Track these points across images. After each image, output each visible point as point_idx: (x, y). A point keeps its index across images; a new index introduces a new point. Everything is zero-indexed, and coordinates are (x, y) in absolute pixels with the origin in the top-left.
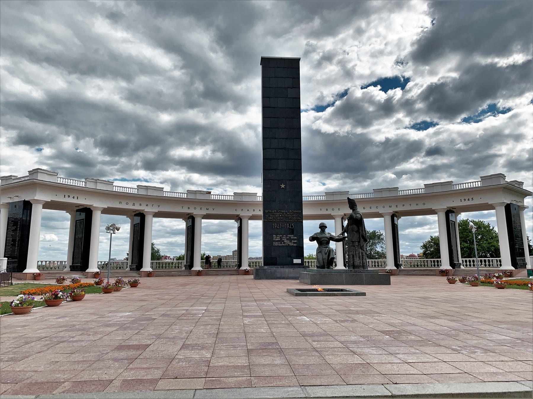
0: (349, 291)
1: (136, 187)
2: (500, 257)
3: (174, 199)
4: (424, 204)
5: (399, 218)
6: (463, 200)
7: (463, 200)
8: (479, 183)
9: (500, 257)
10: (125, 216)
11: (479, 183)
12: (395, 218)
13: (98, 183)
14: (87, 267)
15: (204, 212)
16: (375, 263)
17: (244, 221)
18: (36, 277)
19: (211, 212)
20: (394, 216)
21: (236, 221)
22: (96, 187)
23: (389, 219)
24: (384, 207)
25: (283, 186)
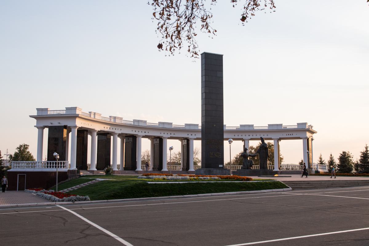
0: (74, 193)
1: (158, 123)
2: (18, 190)
3: (257, 131)
4: (267, 135)
5: (280, 141)
6: (288, 135)
7: (288, 135)
8: (296, 126)
9: (274, 165)
10: (178, 140)
11: (296, 126)
12: (279, 141)
13: (140, 122)
14: (162, 169)
15: (250, 138)
16: (234, 167)
17: (191, 142)
18: (167, 174)
19: (173, 135)
20: (280, 139)
21: (243, 141)
22: (139, 124)
23: (277, 141)
24: (245, 135)
25: (215, 126)
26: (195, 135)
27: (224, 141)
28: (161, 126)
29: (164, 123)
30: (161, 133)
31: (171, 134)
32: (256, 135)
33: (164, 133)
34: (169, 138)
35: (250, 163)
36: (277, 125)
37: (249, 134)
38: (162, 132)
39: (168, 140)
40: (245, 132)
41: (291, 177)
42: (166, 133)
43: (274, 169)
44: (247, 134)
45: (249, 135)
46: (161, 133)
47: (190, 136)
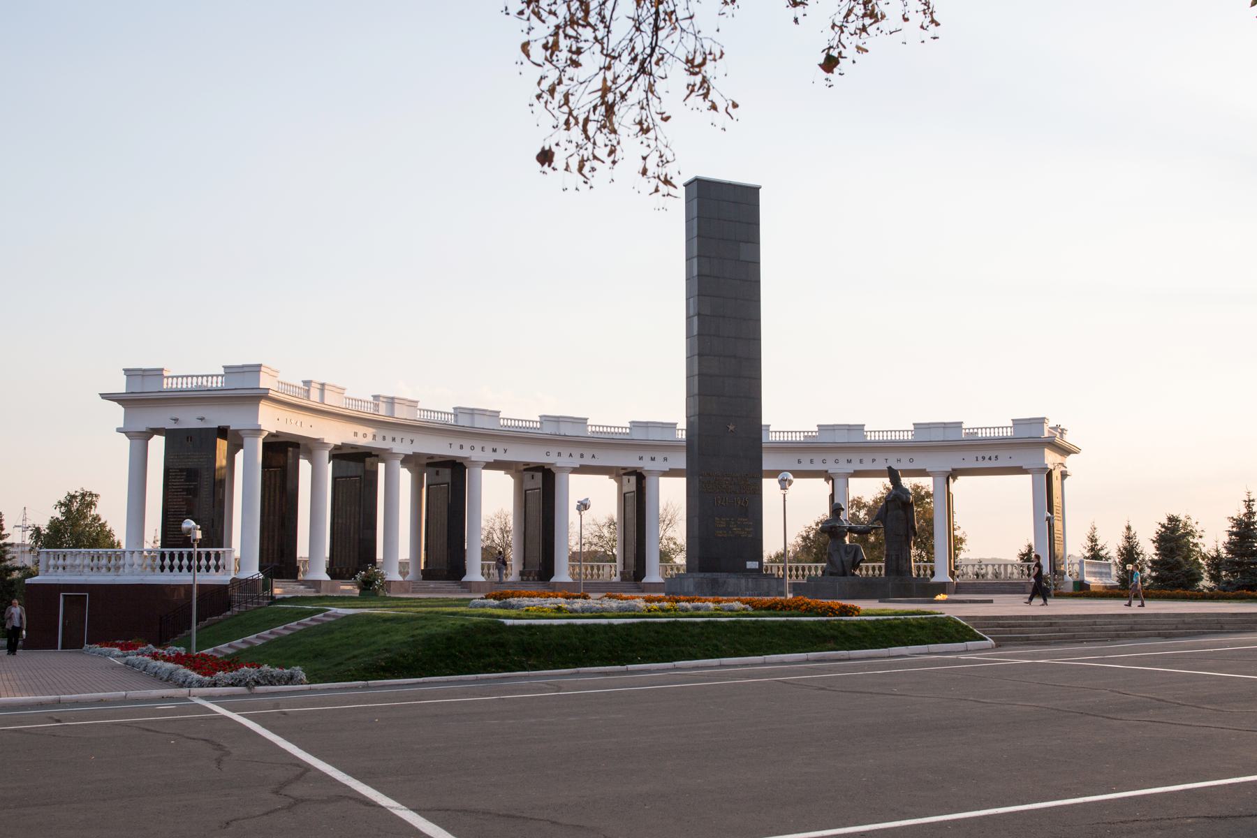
4: (911, 460)
15: (577, 462)
17: (649, 482)
19: (588, 461)
23: (943, 480)
24: (836, 461)
25: (731, 428)
26: (665, 459)
27: (765, 481)
28: (549, 429)
29: (557, 420)
30: (548, 454)
31: (582, 456)
32: (874, 460)
33: (559, 454)
34: (576, 471)
35: (852, 555)
36: (945, 426)
37: (849, 456)
38: (554, 451)
39: (573, 478)
40: (832, 451)
41: (991, 601)
42: (565, 452)
43: (933, 574)
44: (843, 457)
45: (849, 461)
46: (548, 454)
47: (646, 465)
